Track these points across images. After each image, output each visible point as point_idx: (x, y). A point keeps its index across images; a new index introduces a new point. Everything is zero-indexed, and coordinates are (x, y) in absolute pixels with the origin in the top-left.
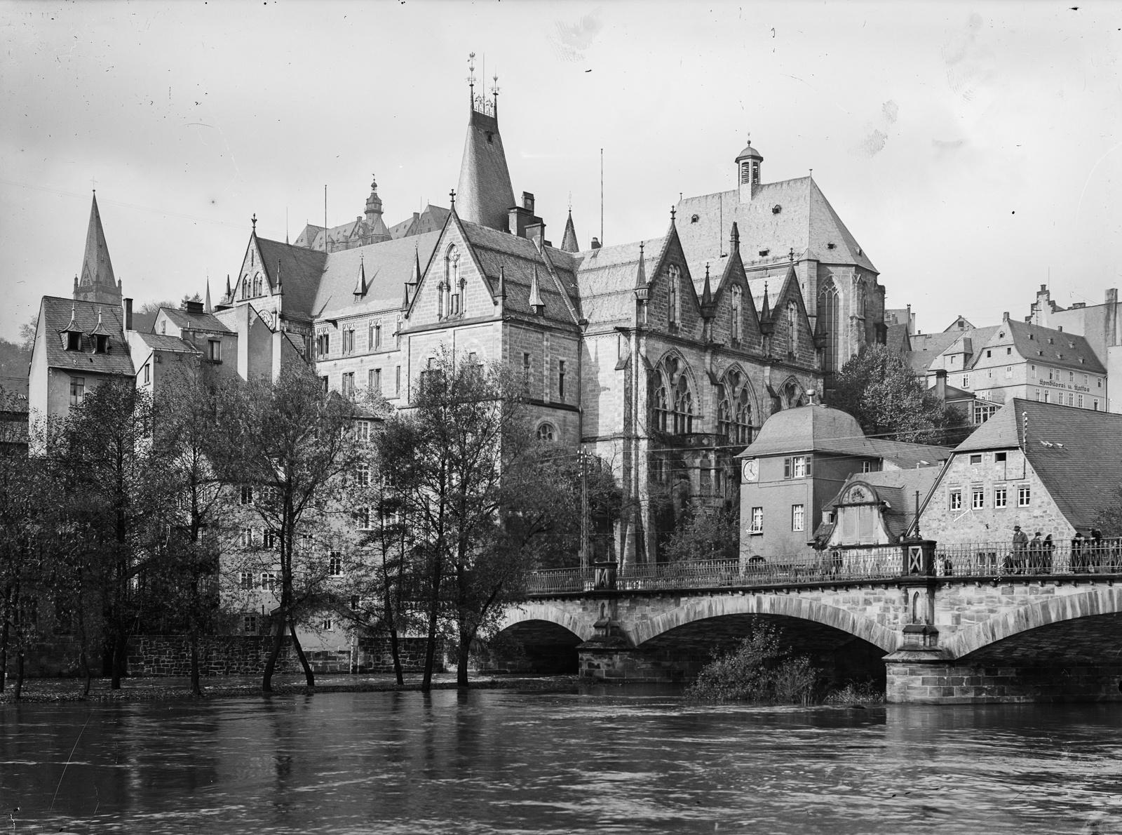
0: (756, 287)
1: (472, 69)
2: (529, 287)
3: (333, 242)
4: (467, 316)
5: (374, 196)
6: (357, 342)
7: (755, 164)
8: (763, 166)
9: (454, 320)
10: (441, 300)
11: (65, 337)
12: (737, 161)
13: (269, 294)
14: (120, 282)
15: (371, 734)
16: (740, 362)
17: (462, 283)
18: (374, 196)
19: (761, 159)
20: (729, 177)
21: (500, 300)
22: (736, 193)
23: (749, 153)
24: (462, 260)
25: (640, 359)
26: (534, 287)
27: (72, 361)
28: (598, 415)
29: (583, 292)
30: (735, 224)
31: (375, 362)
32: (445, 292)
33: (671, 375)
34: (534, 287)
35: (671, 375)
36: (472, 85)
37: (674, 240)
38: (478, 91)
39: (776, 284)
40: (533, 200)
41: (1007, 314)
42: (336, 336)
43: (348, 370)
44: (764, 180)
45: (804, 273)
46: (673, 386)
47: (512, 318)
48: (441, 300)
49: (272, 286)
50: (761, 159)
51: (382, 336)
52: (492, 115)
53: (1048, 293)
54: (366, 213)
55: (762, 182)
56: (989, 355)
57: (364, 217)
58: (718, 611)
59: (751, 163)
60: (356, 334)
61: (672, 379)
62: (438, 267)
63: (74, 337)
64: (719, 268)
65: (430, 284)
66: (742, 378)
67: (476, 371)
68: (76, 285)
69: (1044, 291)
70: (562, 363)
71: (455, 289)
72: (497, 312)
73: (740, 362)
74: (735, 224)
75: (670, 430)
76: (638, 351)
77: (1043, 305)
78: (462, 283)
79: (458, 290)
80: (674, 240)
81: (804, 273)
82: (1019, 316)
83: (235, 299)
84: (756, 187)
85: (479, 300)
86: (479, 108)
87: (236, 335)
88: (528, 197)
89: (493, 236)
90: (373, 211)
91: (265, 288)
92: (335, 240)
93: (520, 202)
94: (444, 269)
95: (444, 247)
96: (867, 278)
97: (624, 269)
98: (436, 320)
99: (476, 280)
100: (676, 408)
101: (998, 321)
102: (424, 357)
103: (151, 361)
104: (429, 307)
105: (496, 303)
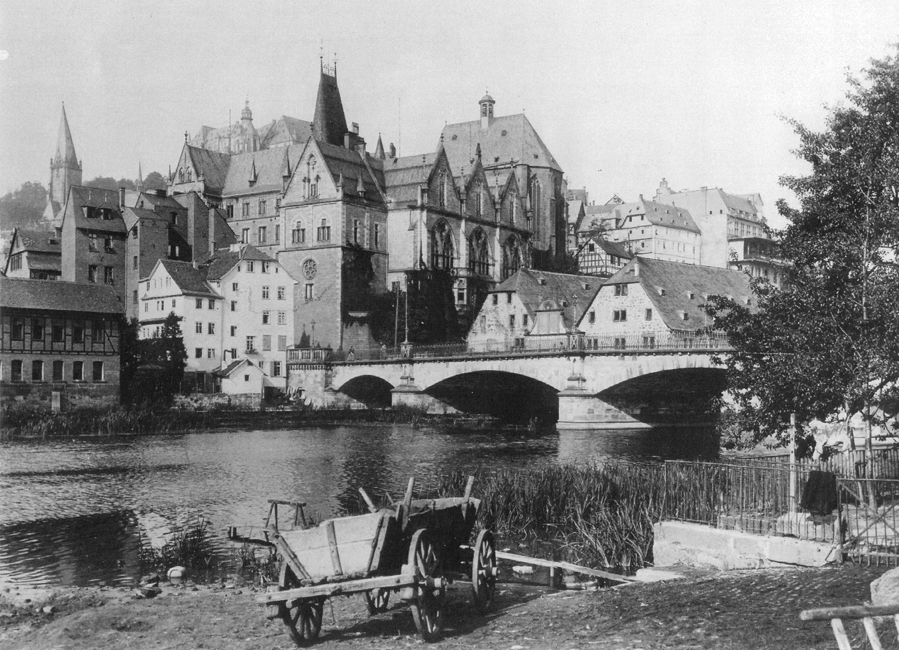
0: (491, 180)
1: (322, 48)
2: (357, 181)
3: (220, 138)
4: (321, 198)
5: (247, 109)
6: (251, 210)
7: (490, 105)
8: (495, 106)
9: (313, 200)
10: (305, 188)
11: (85, 209)
12: (480, 103)
13: (196, 181)
14: (81, 162)
15: (206, 540)
16: (482, 226)
17: (318, 178)
18: (247, 109)
19: (494, 102)
20: (475, 113)
21: (340, 189)
22: (479, 123)
23: (487, 99)
24: (317, 164)
25: (423, 224)
26: (360, 180)
27: (93, 224)
28: (36, 184)
29: (387, 184)
30: (479, 144)
31: (265, 222)
32: (307, 183)
33: (441, 233)
34: (360, 180)
35: (441, 233)
36: (321, 57)
37: (443, 154)
38: (325, 63)
39: (503, 179)
40: (358, 128)
41: (641, 195)
42: (238, 207)
43: (245, 227)
44: (496, 114)
45: (520, 172)
46: (442, 240)
47: (350, 198)
48: (305, 188)
49: (198, 175)
50: (494, 102)
51: (331, 233)
52: (334, 76)
53: (667, 183)
54: (242, 119)
55: (495, 116)
56: (631, 220)
57: (241, 122)
58: (496, 368)
59: (487, 105)
60: (251, 205)
61: (441, 236)
62: (303, 169)
63: (91, 210)
64: (469, 171)
65: (297, 179)
66: (483, 235)
67: (541, 308)
68: (52, 163)
69: (664, 182)
70: (376, 226)
71: (313, 182)
72: (340, 195)
73: (482, 226)
74: (479, 144)
75: (440, 266)
76: (421, 219)
77: (664, 191)
78: (318, 178)
79: (315, 182)
80: (443, 154)
81: (520, 172)
82: (648, 198)
83: (174, 183)
84: (492, 119)
85: (329, 188)
86: (325, 71)
87: (187, 209)
88: (355, 126)
89: (334, 150)
90: (247, 119)
91: (194, 177)
92: (221, 136)
93: (350, 128)
94: (307, 169)
95: (307, 156)
96: (557, 175)
97: (413, 170)
98: (302, 200)
99: (326, 176)
100: (444, 253)
101: (637, 200)
102: (294, 221)
103: (138, 225)
104: (298, 191)
105: (338, 191)
